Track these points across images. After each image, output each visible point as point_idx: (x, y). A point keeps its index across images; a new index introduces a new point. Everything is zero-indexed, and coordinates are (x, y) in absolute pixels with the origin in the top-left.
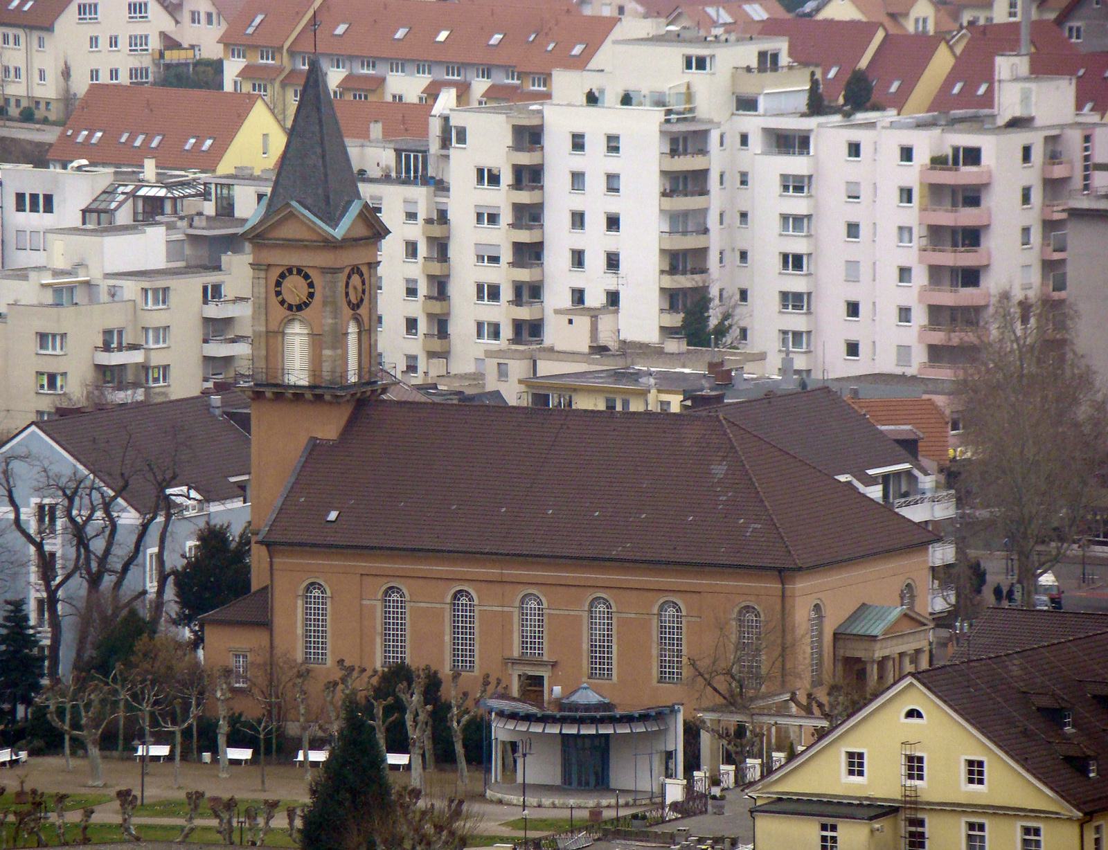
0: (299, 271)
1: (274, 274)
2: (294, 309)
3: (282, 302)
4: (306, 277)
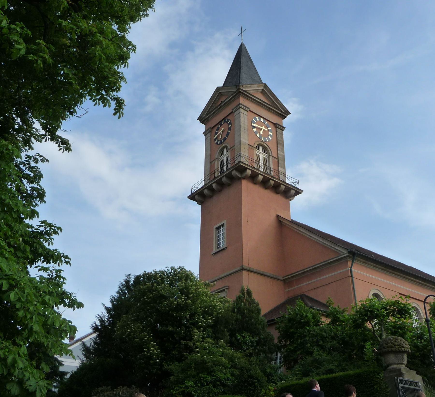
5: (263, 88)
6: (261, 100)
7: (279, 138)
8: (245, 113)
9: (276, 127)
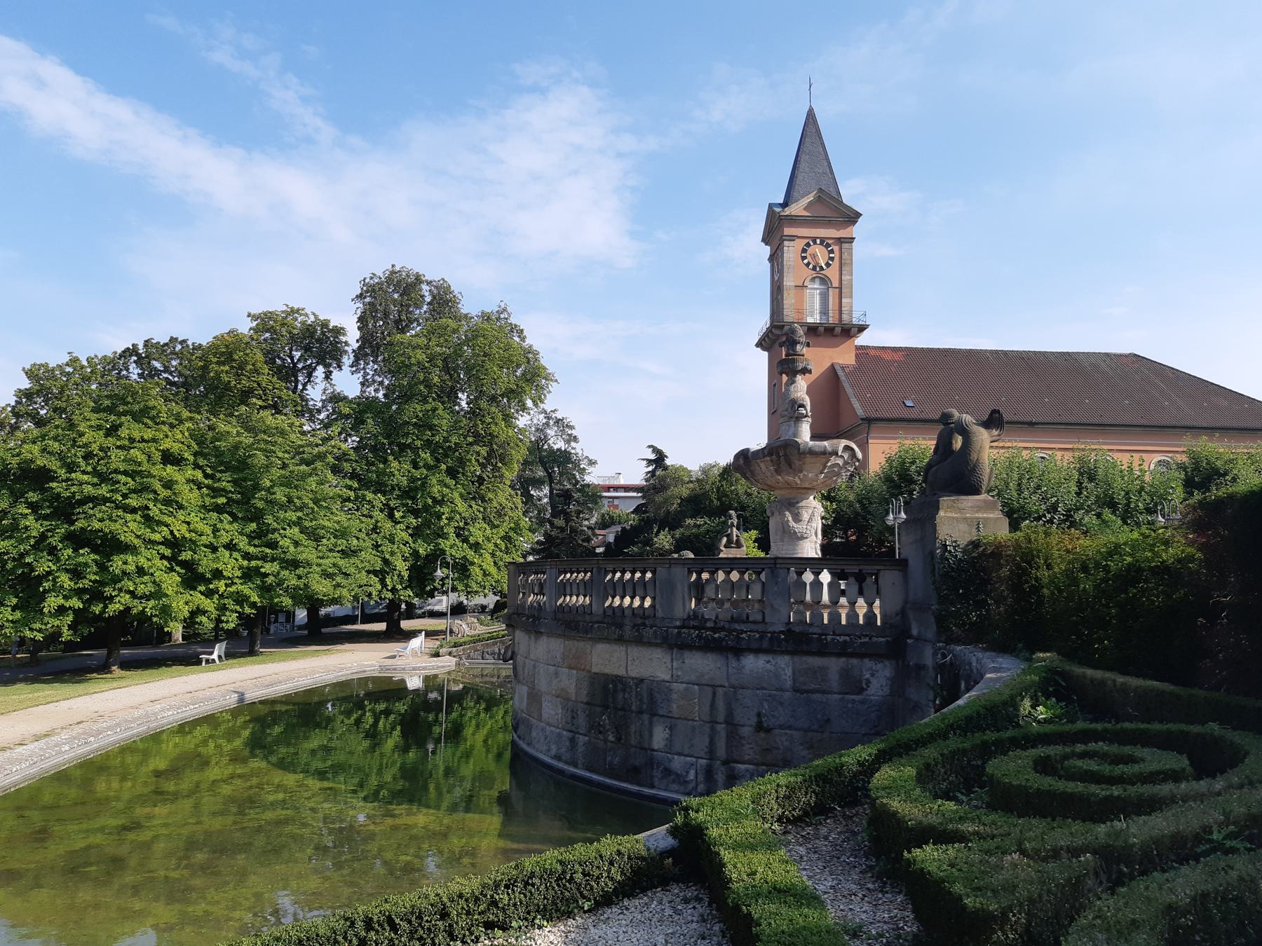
7: (845, 256)
8: (791, 243)
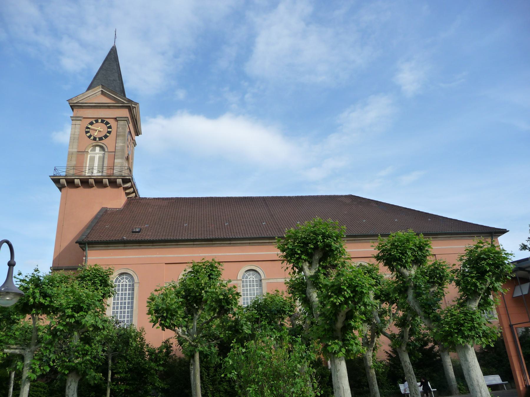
0: (102, 121)
1: (86, 122)
2: (97, 139)
3: (90, 137)
4: (107, 123)
5: (101, 89)
6: (95, 103)
9: (117, 121)
